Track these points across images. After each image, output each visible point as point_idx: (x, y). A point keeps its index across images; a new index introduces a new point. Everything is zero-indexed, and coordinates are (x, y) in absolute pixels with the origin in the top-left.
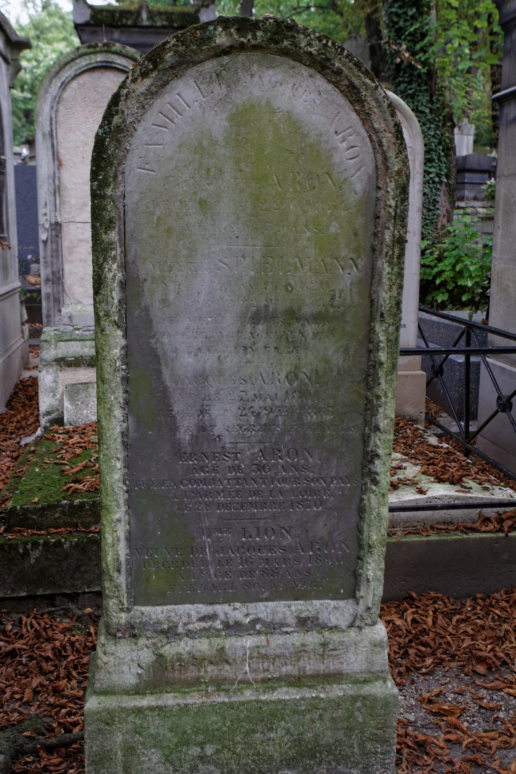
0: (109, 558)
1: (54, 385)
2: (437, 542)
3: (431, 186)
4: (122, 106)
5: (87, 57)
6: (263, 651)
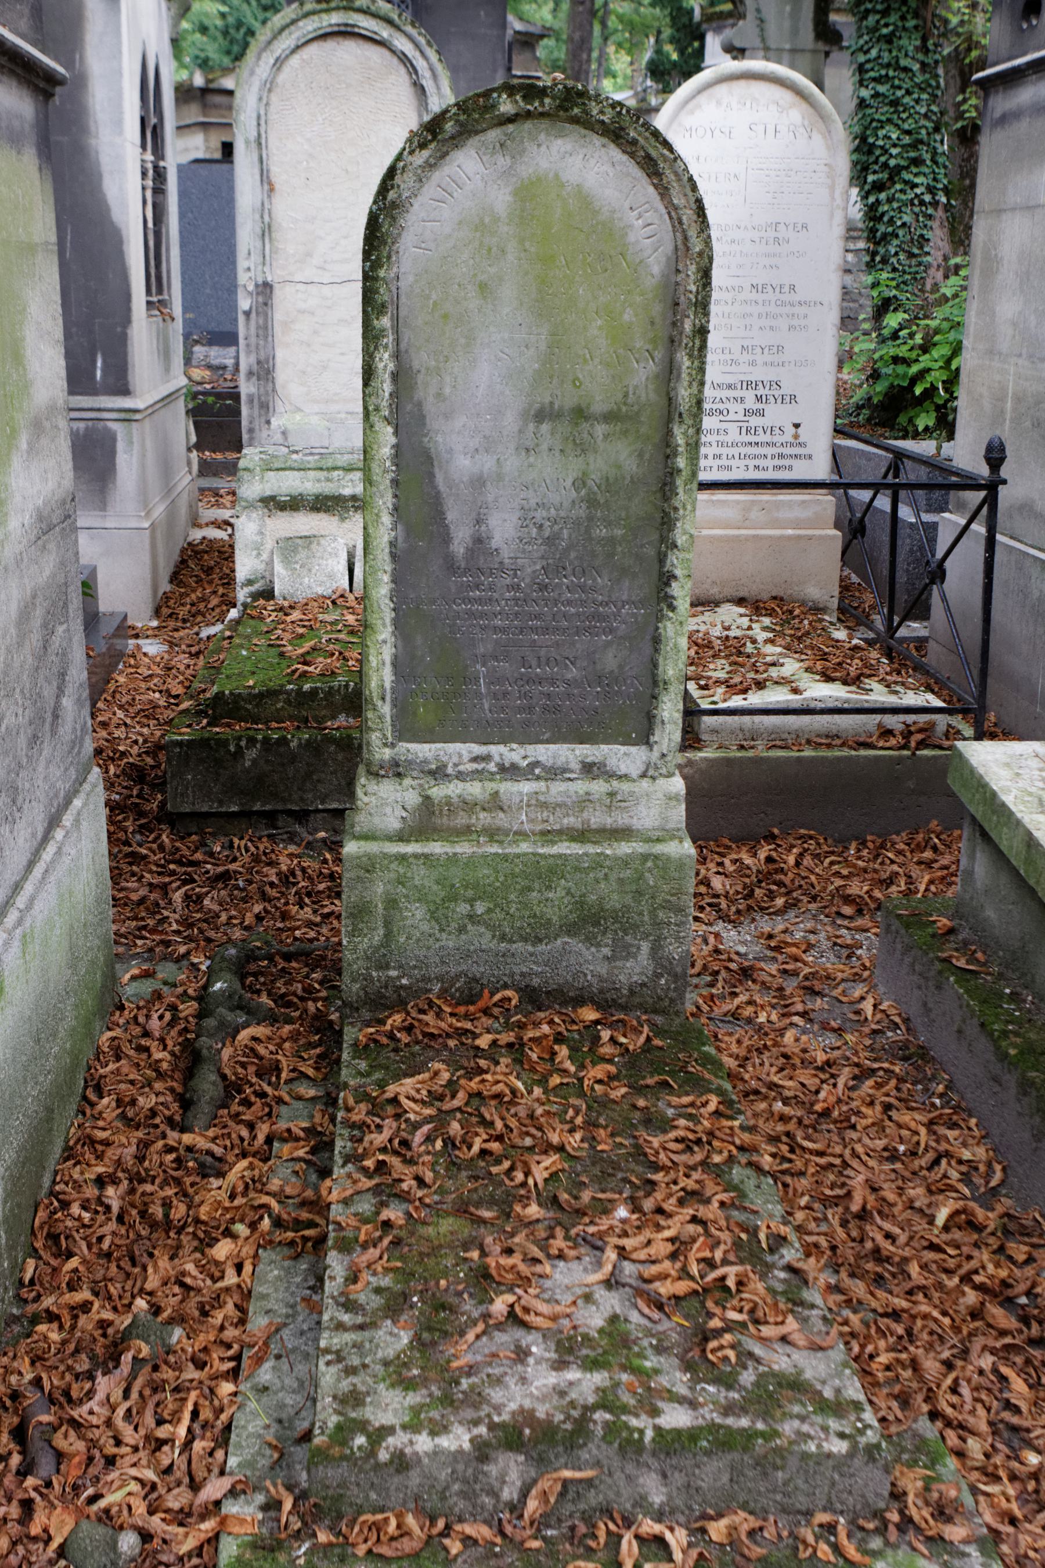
0: (373, 684)
1: (258, 538)
2: (812, 759)
3: (917, 209)
4: (398, 180)
5: (316, 18)
6: (542, 798)
